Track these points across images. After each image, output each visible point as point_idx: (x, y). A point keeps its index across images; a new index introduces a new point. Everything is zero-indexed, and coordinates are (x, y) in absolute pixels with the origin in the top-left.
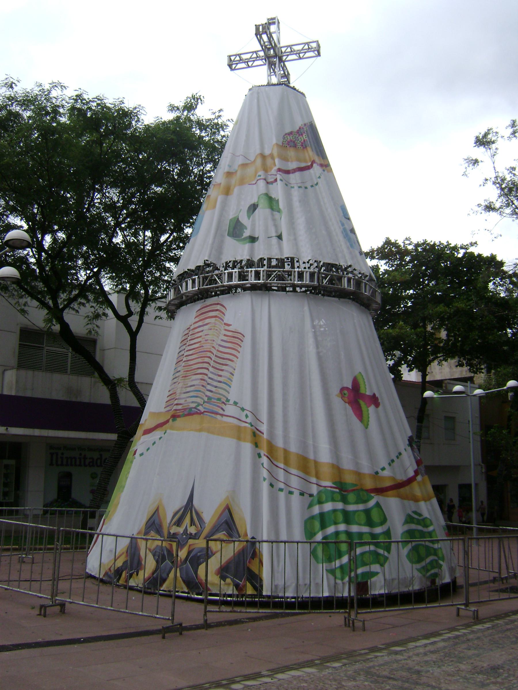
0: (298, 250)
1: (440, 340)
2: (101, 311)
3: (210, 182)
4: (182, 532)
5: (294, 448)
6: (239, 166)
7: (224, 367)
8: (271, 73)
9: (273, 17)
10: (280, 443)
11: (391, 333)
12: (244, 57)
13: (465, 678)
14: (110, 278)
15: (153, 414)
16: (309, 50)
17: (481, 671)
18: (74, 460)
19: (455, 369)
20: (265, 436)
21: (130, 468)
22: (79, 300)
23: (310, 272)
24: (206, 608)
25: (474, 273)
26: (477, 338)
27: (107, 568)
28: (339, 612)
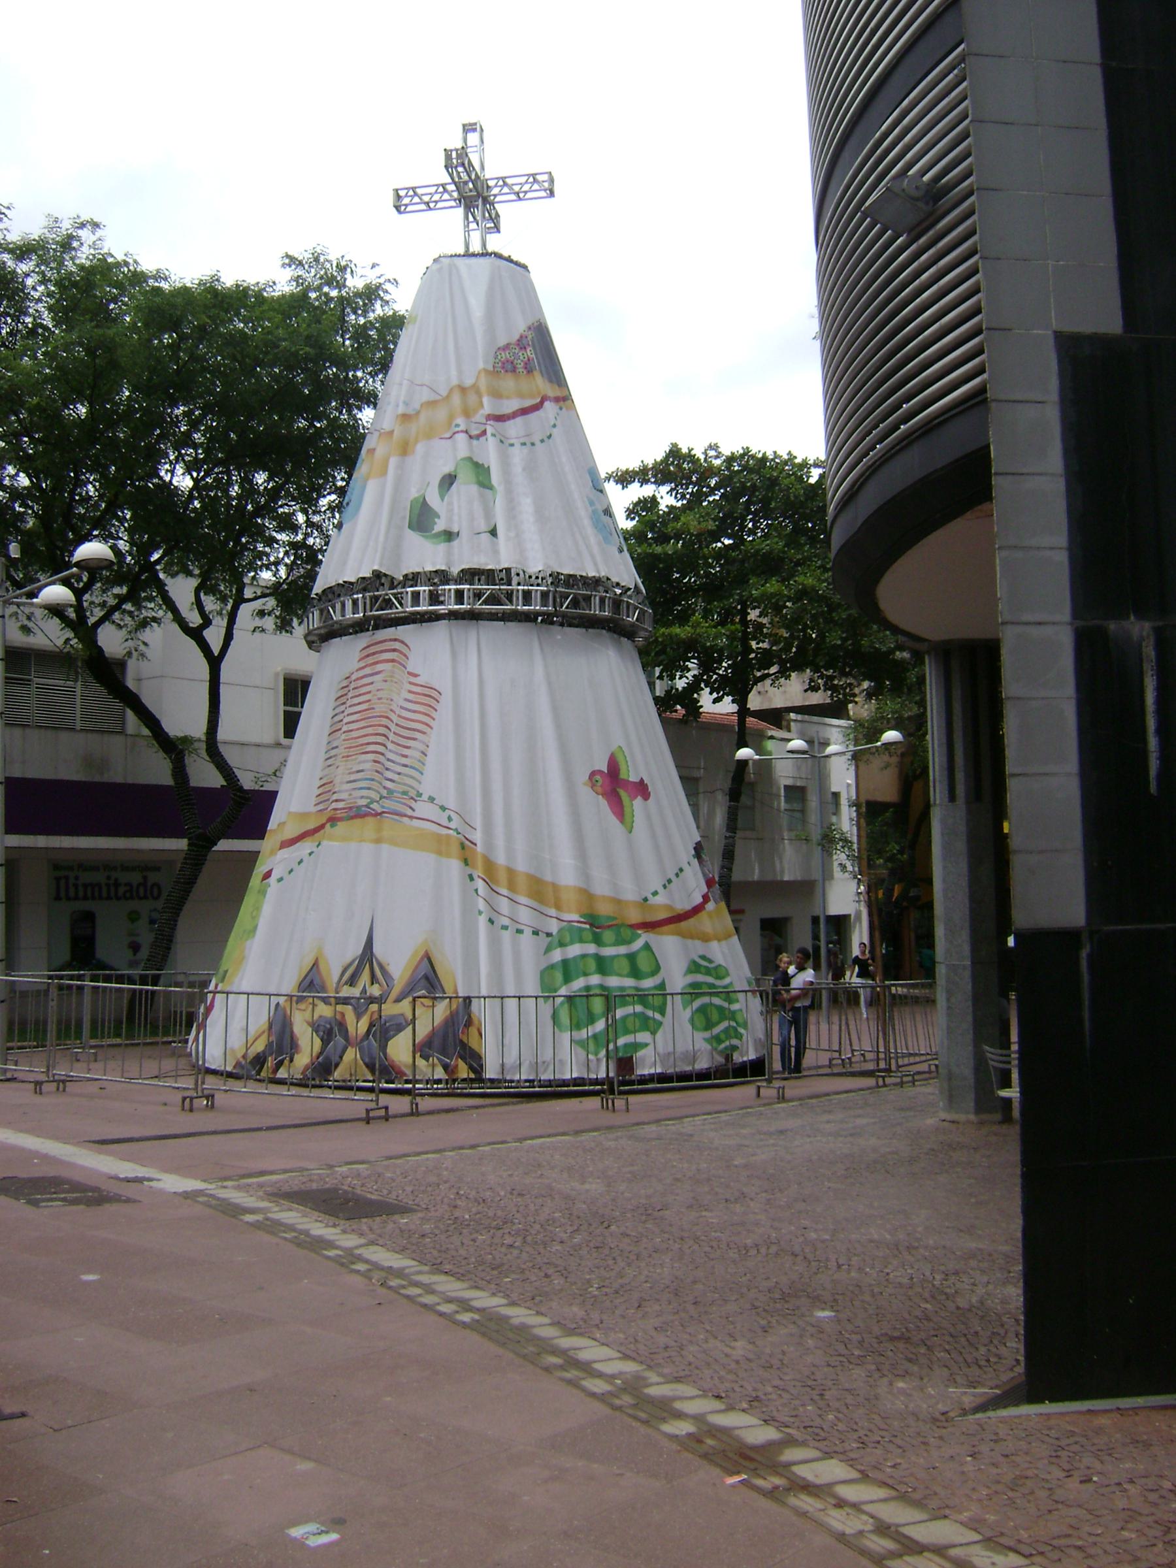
9: (472, 121)
10: (501, 859)
18: (97, 889)
27: (239, 1055)
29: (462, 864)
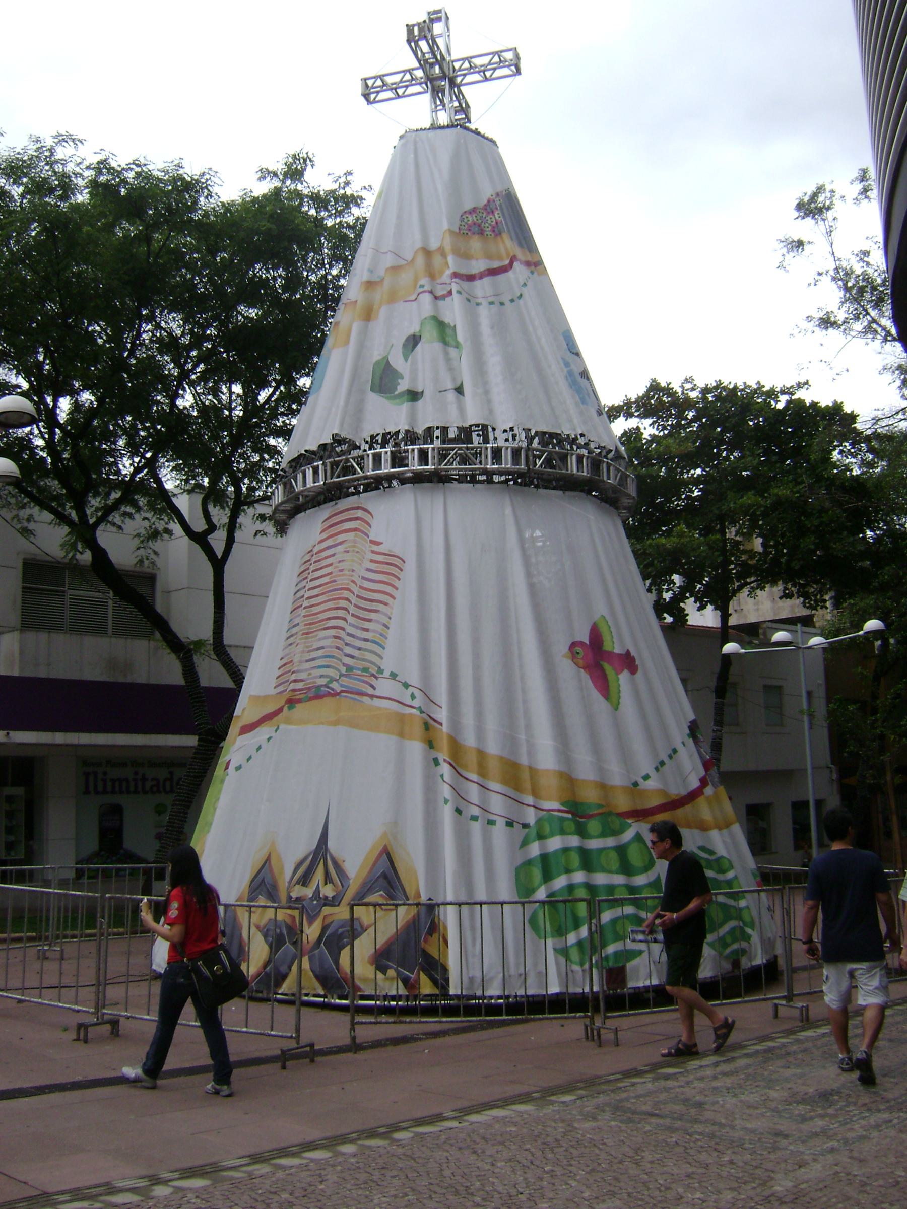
0: (491, 411)
1: (752, 553)
2: (160, 526)
3: (339, 297)
4: (311, 895)
5: (493, 747)
6: (387, 270)
7: (372, 616)
8: (436, 107)
10: (469, 740)
11: (663, 545)
12: (389, 80)
13: (775, 1110)
14: (174, 469)
15: (255, 699)
16: (502, 63)
17: (803, 1099)
19: (781, 603)
20: (445, 728)
21: (220, 792)
22: (123, 509)
23: (513, 449)
24: (353, 1018)
25: (805, 435)
26: (813, 547)
28: (575, 1017)
29: (427, 747)
